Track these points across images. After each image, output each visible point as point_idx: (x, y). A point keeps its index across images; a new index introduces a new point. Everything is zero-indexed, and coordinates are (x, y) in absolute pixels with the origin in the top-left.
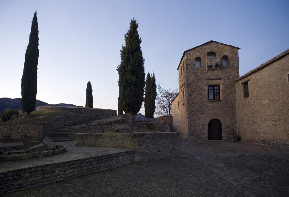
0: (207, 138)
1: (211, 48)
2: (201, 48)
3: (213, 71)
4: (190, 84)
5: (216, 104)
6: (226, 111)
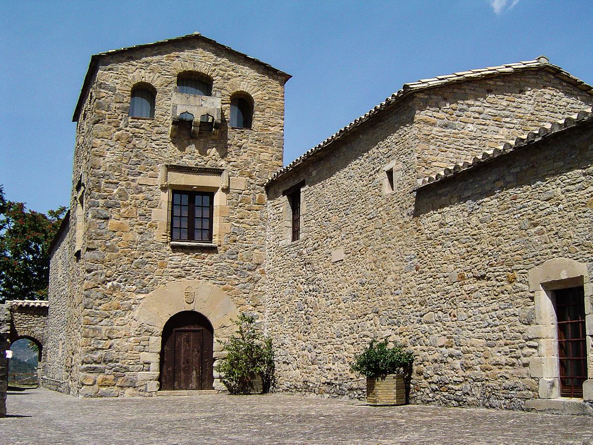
4: (104, 176)
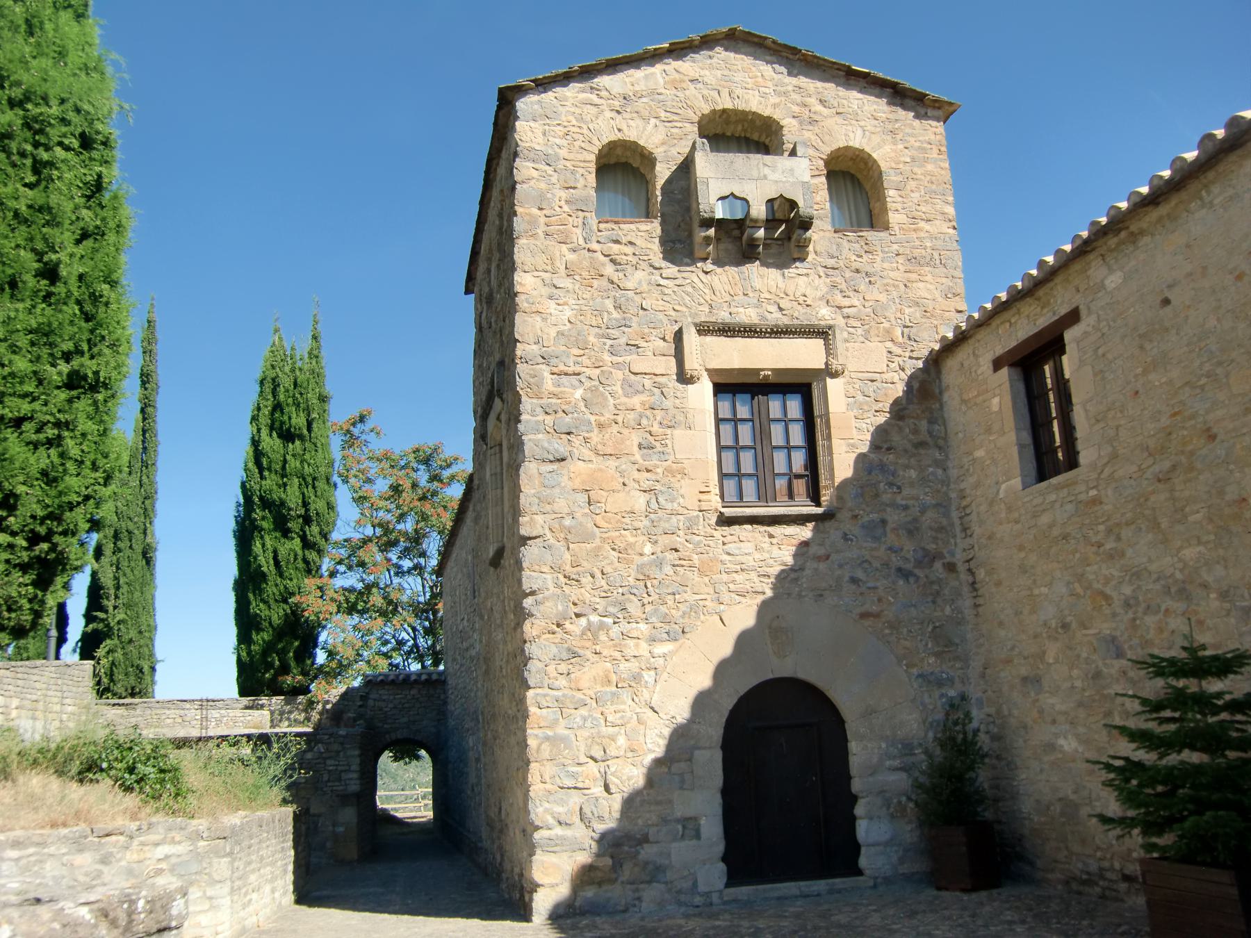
6: (875, 608)
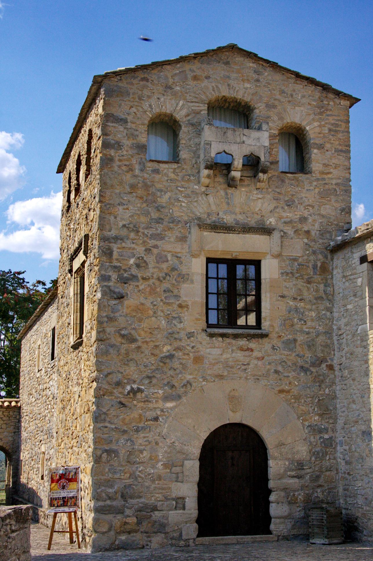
0: (196, 525)
1: (229, 77)
2: (176, 70)
3: (230, 191)
4: (116, 239)
5: (241, 349)
